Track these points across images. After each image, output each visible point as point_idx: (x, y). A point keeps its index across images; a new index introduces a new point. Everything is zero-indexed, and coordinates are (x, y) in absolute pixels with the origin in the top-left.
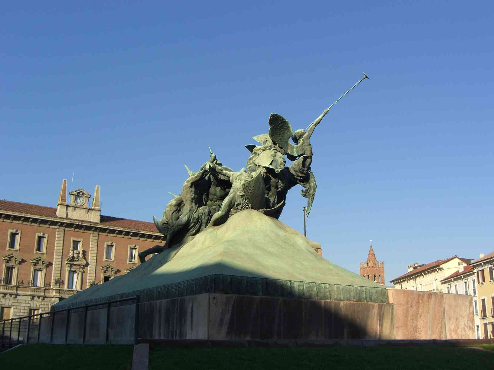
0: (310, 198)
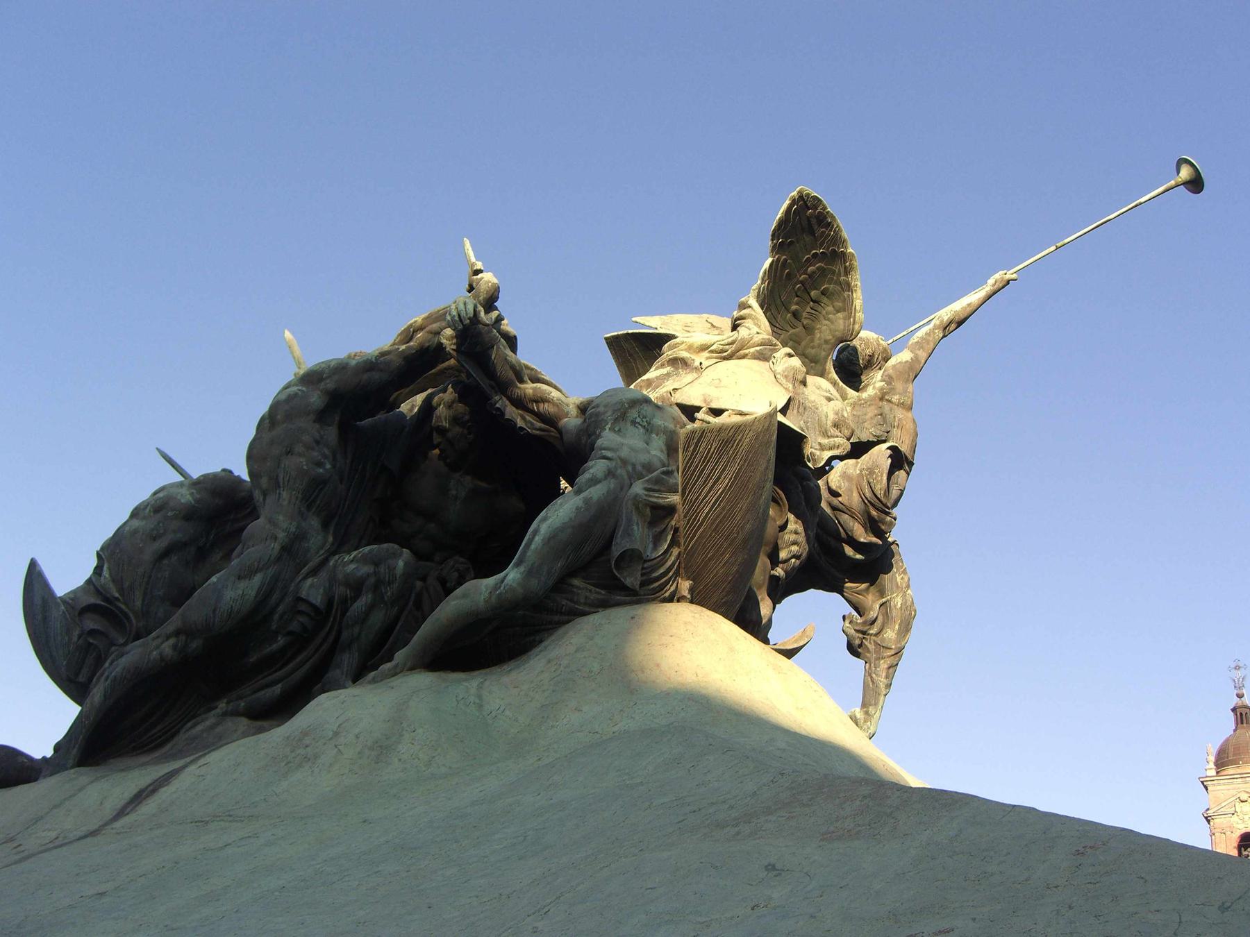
0: (884, 665)
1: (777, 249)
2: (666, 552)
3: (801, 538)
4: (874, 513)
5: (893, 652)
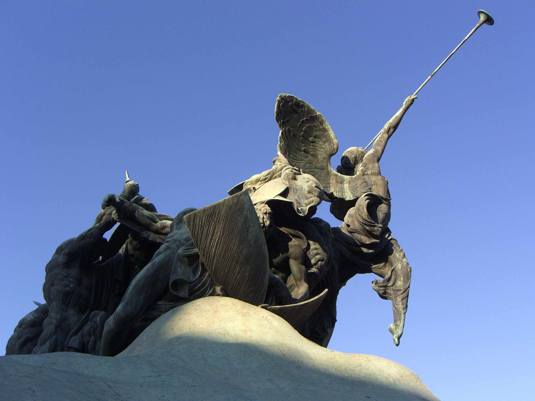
0: (399, 299)
1: (282, 125)
2: (200, 276)
3: (320, 251)
4: (367, 228)
5: (402, 291)
